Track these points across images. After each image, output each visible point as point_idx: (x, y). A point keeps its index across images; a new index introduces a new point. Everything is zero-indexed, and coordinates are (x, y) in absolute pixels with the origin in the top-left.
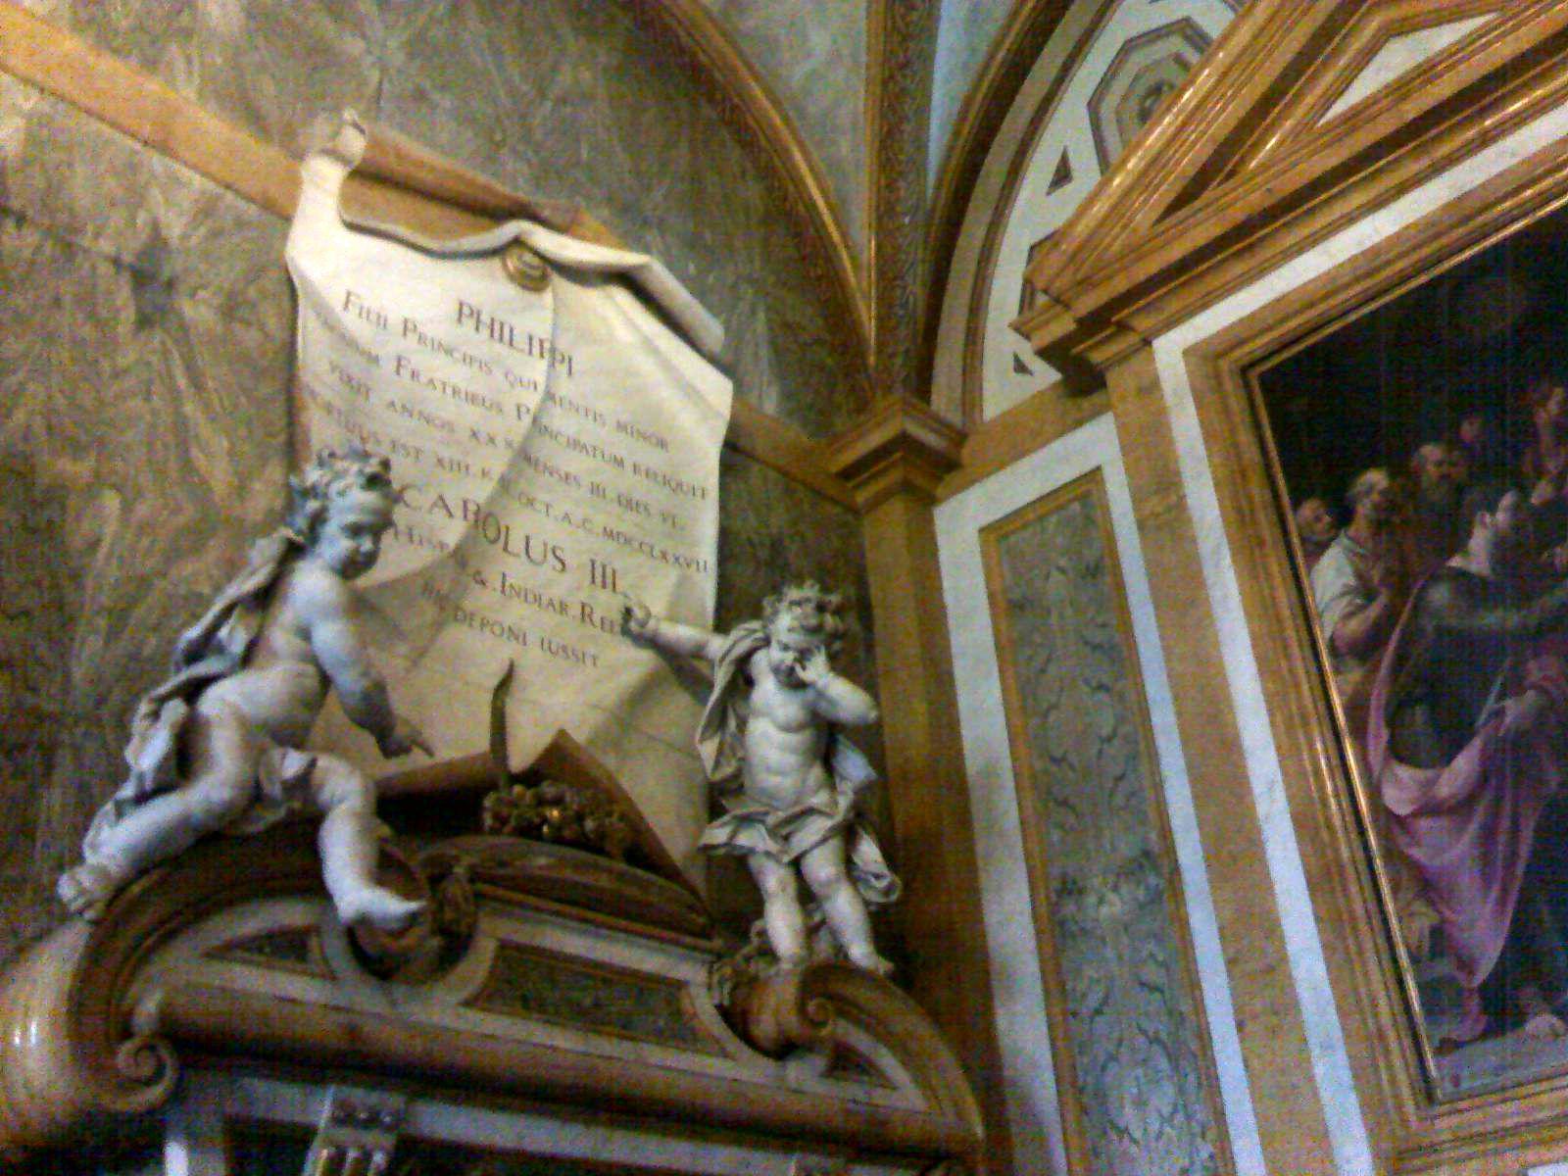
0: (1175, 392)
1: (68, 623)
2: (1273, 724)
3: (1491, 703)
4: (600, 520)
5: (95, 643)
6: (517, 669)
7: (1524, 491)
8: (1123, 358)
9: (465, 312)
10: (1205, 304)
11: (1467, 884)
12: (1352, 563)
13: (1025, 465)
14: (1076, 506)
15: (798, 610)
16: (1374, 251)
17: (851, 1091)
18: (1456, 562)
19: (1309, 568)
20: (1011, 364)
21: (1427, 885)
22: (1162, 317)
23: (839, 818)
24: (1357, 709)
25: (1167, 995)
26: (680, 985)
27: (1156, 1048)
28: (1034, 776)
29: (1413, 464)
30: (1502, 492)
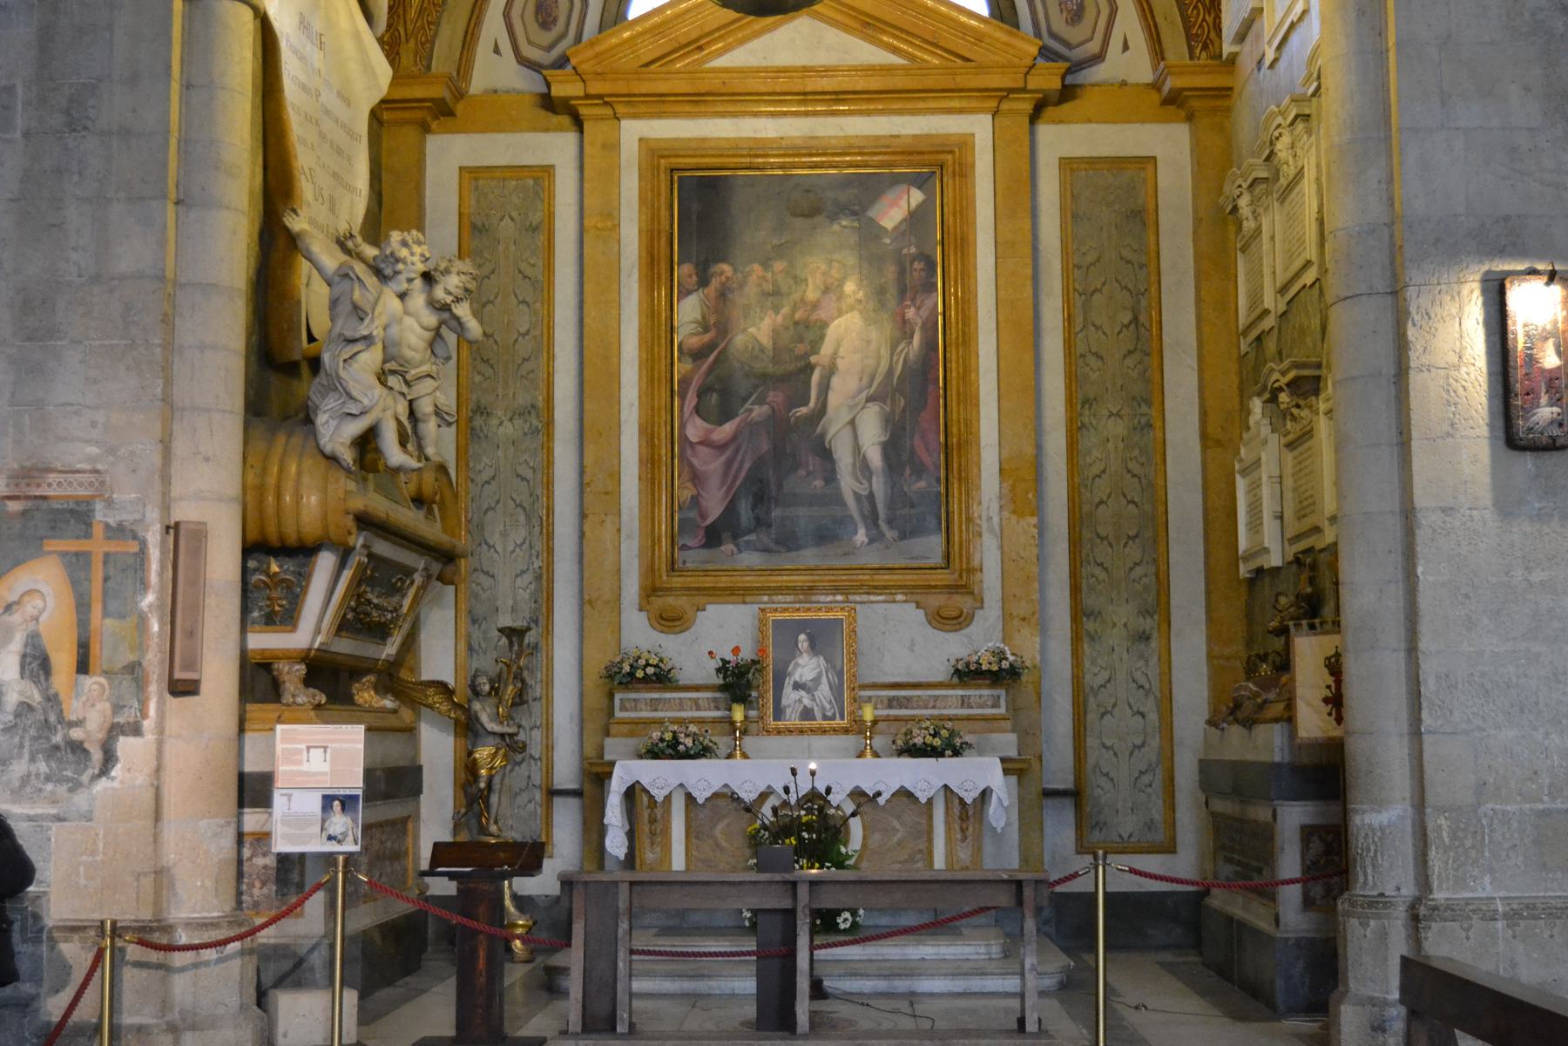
2: (640, 376)
3: (747, 405)
11: (714, 482)
13: (501, 138)
14: (531, 182)
21: (696, 478)
24: (685, 382)
27: (519, 510)
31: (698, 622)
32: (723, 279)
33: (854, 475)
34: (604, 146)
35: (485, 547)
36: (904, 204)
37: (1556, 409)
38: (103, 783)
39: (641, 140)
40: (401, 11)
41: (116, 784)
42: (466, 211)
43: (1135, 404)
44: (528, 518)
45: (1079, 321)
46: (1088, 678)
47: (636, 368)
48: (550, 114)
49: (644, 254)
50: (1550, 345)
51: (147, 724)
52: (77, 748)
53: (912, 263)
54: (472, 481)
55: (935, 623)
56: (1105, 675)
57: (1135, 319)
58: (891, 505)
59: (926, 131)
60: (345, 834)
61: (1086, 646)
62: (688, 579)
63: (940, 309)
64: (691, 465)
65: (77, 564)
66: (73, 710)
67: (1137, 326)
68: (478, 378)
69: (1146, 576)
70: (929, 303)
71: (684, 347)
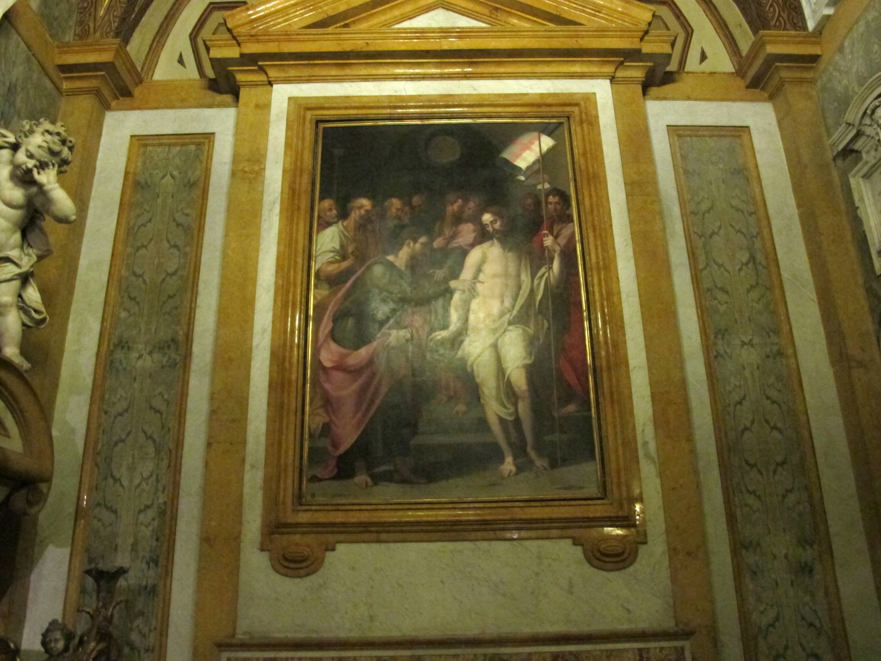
0: (277, 115)
2: (275, 301)
3: (384, 330)
7: (432, 240)
8: (255, 85)
10: (309, 80)
11: (348, 408)
12: (341, 238)
15: (48, 137)
16: (401, 98)
18: (391, 258)
19: (318, 232)
22: (284, 75)
23: (24, 269)
24: (320, 308)
25: (164, 416)
27: (150, 442)
29: (386, 204)
30: (421, 235)
31: (326, 564)
32: (363, 212)
33: (498, 399)
34: (257, 106)
35: (111, 481)
36: (535, 147)
39: (290, 99)
40: (93, 10)
42: (132, 171)
43: (764, 333)
44: (158, 451)
45: (702, 259)
46: (755, 616)
47: (272, 293)
48: (215, 94)
49: (286, 190)
53: (547, 196)
54: (106, 413)
55: (596, 562)
56: (772, 613)
57: (753, 258)
58: (538, 433)
59: (552, 91)
61: (748, 580)
62: (317, 515)
63: (577, 237)
64: (322, 388)
67: (755, 264)
68: (123, 315)
69: (799, 503)
70: (566, 232)
71: (322, 274)
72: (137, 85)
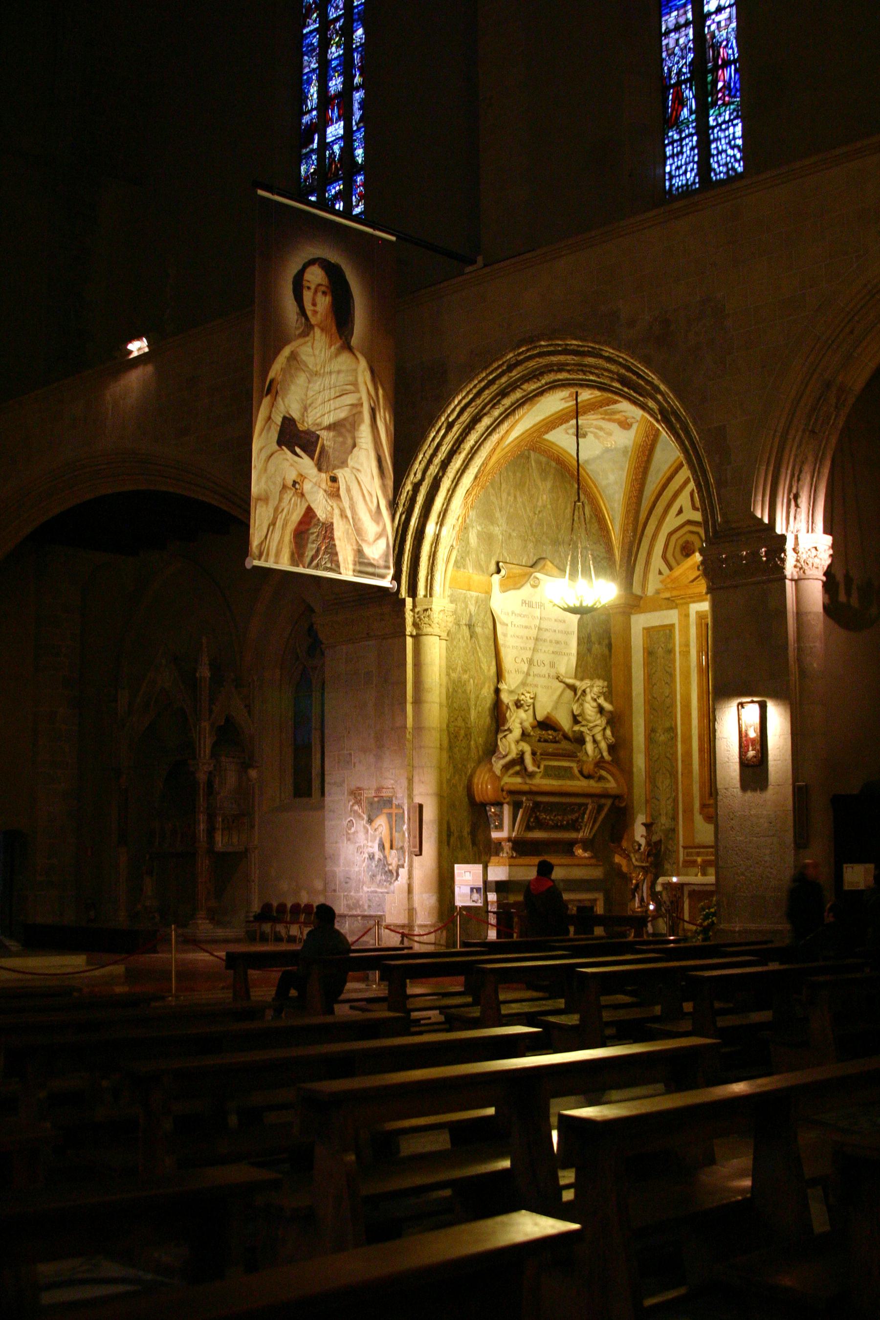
1: (469, 709)
4: (552, 649)
5: (473, 711)
6: (537, 695)
9: (524, 602)
17: (601, 785)
20: (657, 572)
26: (571, 768)
28: (649, 701)
37: (754, 752)
38: (396, 882)
41: (399, 883)
44: (670, 775)
50: (752, 728)
51: (406, 865)
52: (391, 871)
60: (478, 900)
65: (389, 815)
66: (390, 860)
72: (640, 600)
